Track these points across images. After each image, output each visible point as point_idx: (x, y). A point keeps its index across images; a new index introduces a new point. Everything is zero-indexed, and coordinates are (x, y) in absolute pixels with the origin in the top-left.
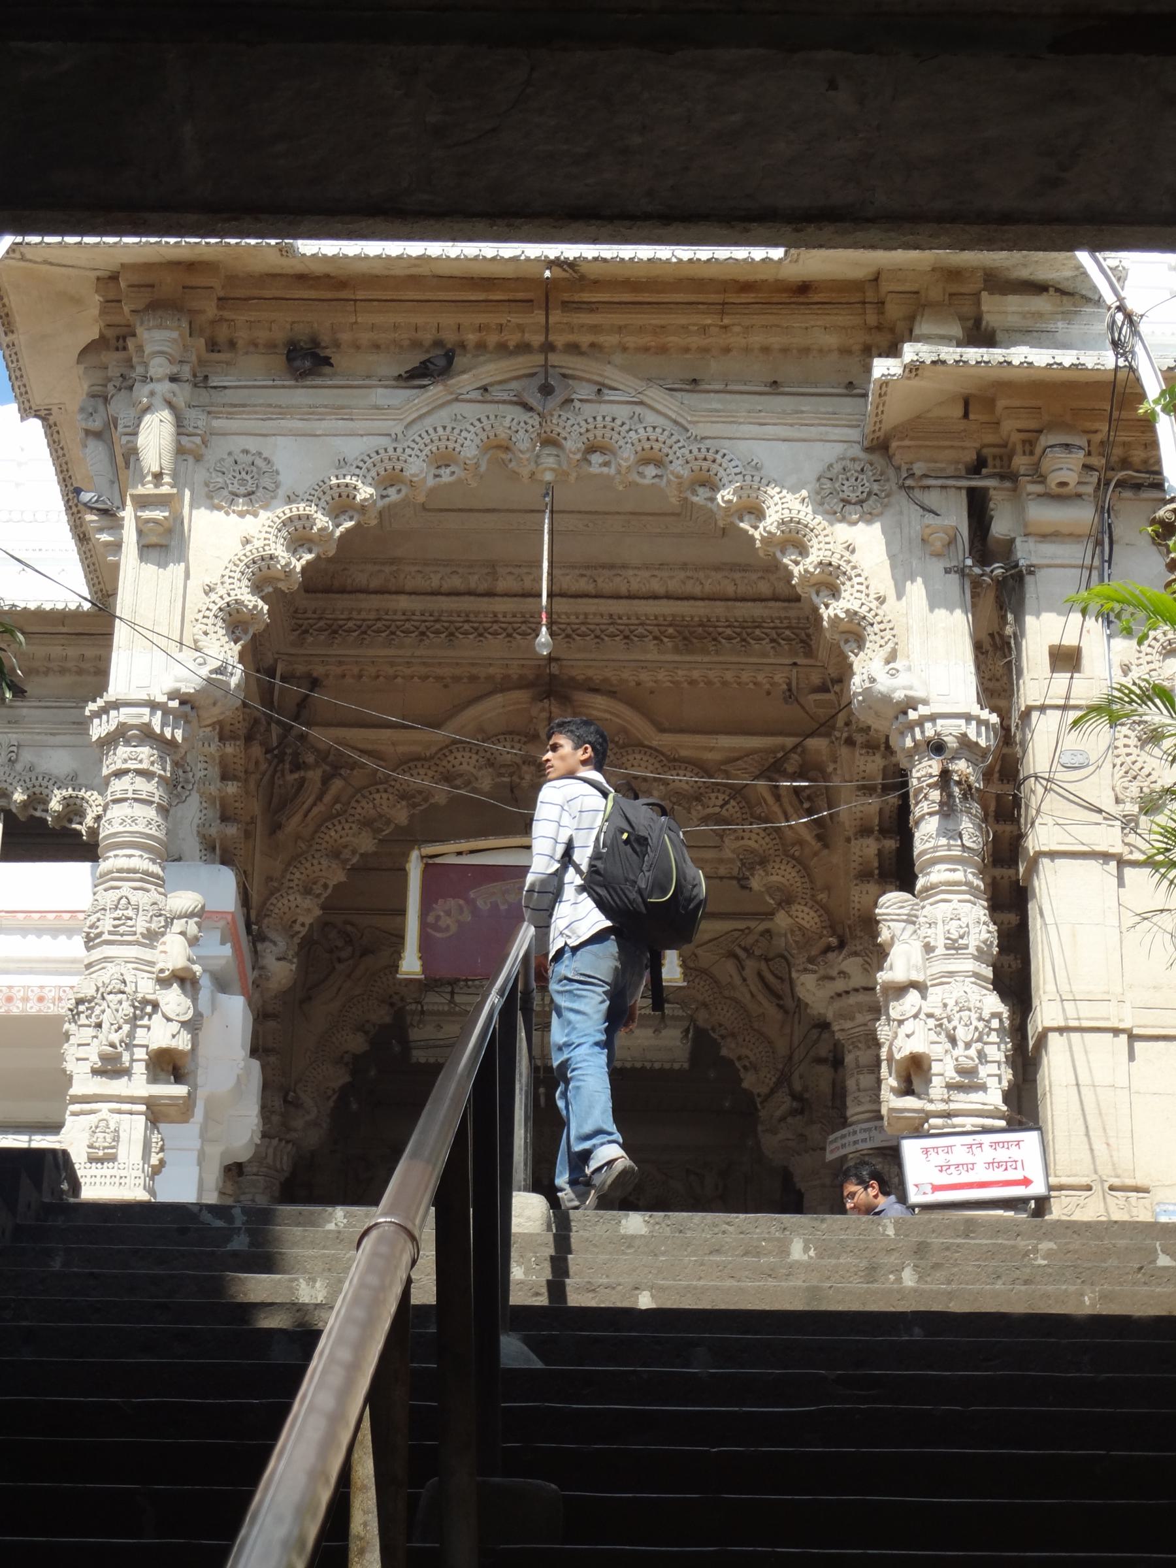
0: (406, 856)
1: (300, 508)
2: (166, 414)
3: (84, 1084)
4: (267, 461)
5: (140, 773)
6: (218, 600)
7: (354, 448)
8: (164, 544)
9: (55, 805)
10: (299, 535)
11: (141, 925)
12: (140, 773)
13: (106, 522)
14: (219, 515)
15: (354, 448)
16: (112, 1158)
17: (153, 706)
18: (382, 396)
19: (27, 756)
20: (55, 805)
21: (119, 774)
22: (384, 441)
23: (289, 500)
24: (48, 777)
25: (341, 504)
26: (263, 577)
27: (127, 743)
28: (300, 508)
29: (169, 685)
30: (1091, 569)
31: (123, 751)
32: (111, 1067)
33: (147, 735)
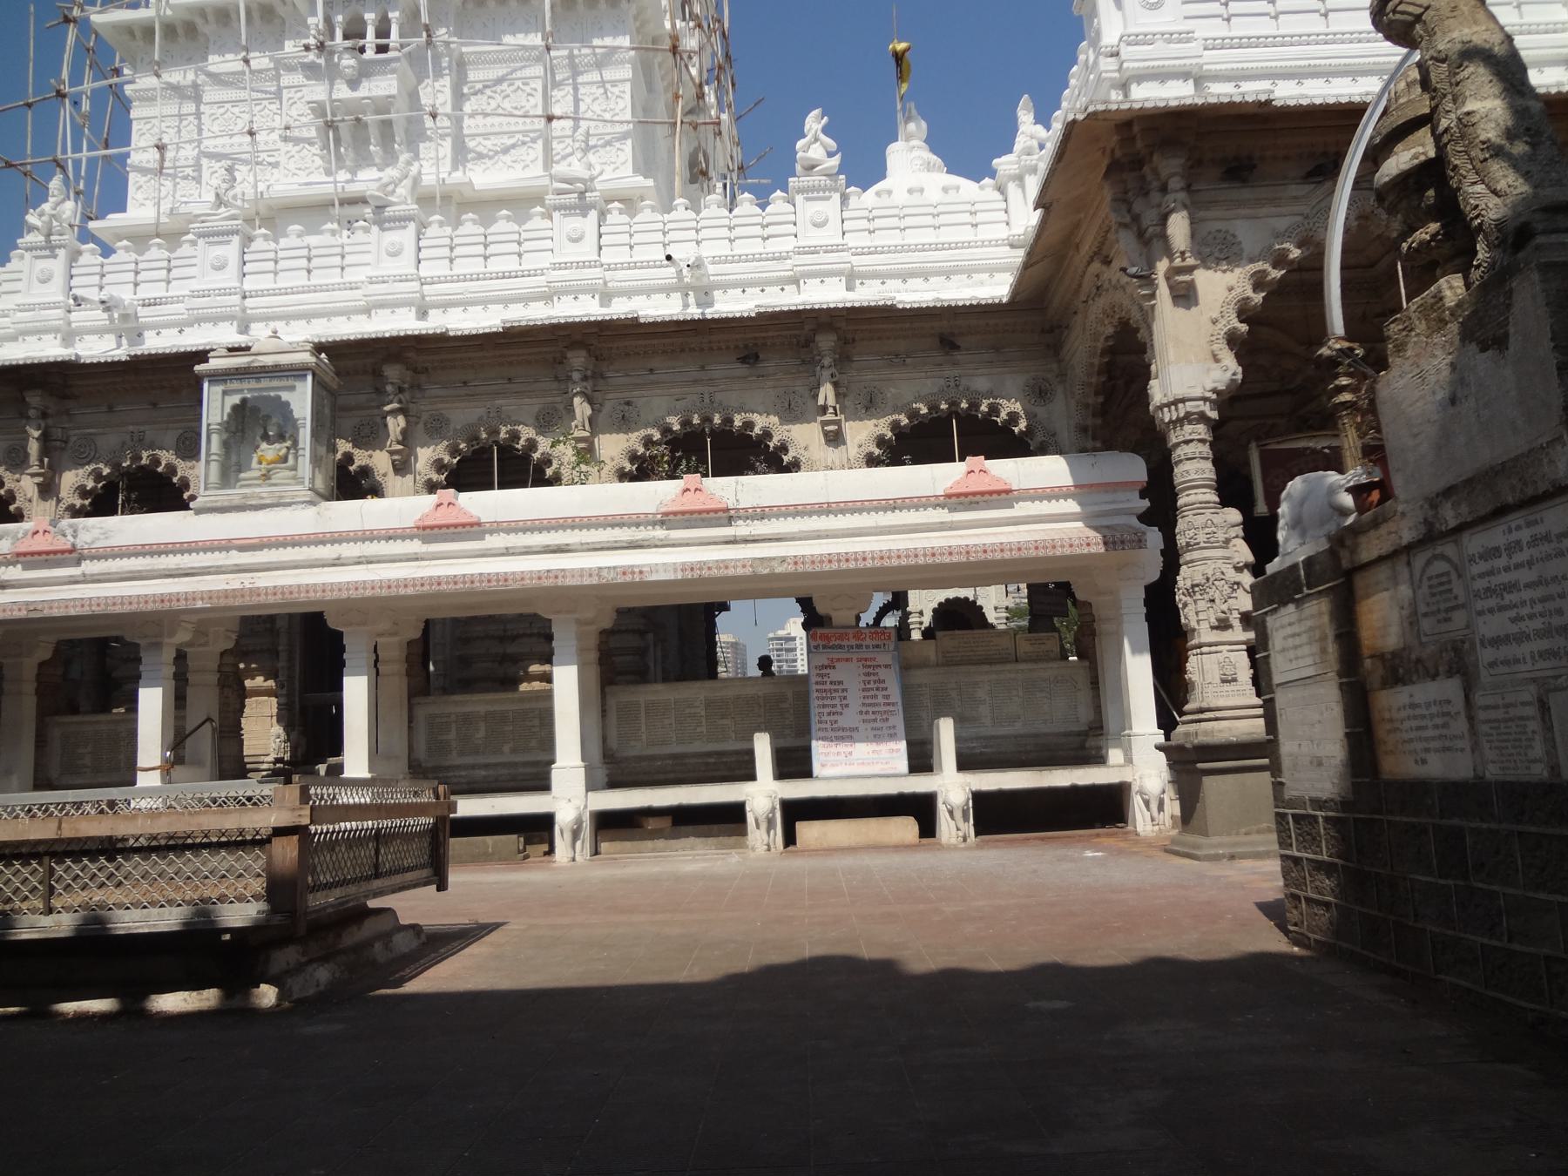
0: (1246, 448)
1: (1260, 266)
2: (1185, 213)
3: (1205, 634)
4: (1234, 236)
5: (1200, 441)
6: (1223, 328)
7: (1282, 224)
8: (1185, 296)
9: (984, 408)
10: (1259, 282)
11: (1221, 536)
12: (1200, 441)
13: (1143, 282)
14: (1210, 272)
15: (1282, 224)
16: (1235, 680)
17: (1205, 399)
18: (1295, 190)
19: (964, 382)
20: (984, 408)
21: (1187, 442)
22: (1299, 219)
23: (1252, 261)
24: (977, 392)
25: (1279, 260)
26: (1244, 312)
27: (1190, 423)
28: (1260, 266)
29: (1210, 386)
30: (603, 83)
31: (1188, 428)
32: (1223, 625)
33: (1202, 418)
